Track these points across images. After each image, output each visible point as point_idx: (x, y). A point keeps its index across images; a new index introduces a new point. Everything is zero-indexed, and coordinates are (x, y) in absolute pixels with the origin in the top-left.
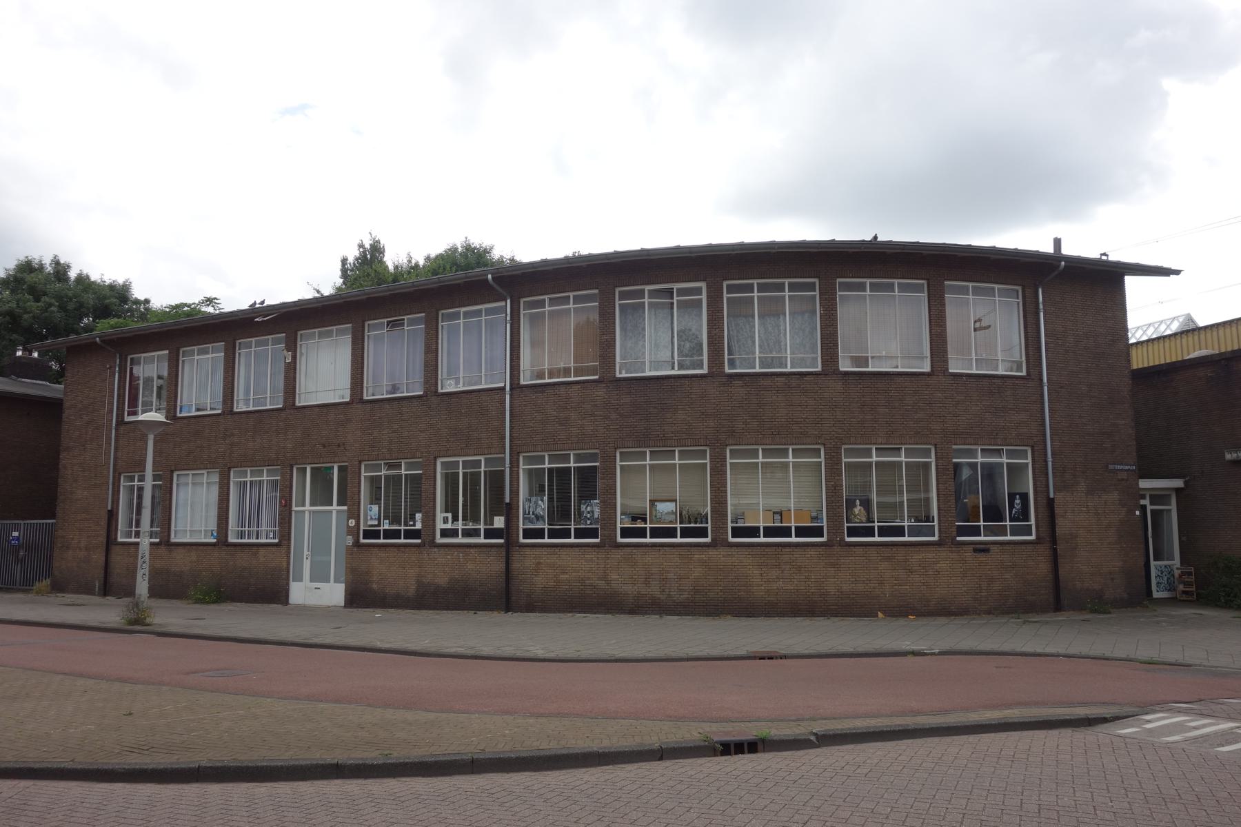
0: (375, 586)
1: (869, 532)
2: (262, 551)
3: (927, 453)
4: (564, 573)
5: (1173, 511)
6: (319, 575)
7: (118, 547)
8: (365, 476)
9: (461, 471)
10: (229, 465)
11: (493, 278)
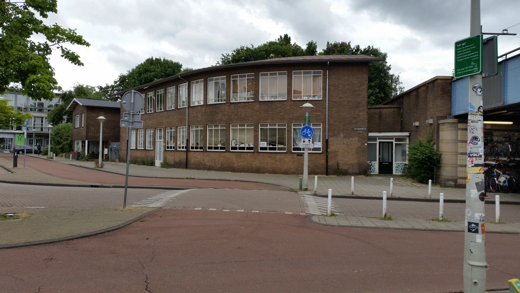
0: (167, 162)
3: (284, 125)
5: (377, 144)
7: (190, 152)
8: (208, 129)
10: (166, 127)
11: (180, 77)
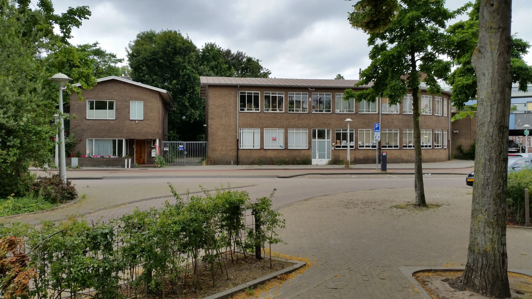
1: (363, 146)
2: (302, 151)
4: (392, 155)
6: (322, 157)
9: (253, 95)
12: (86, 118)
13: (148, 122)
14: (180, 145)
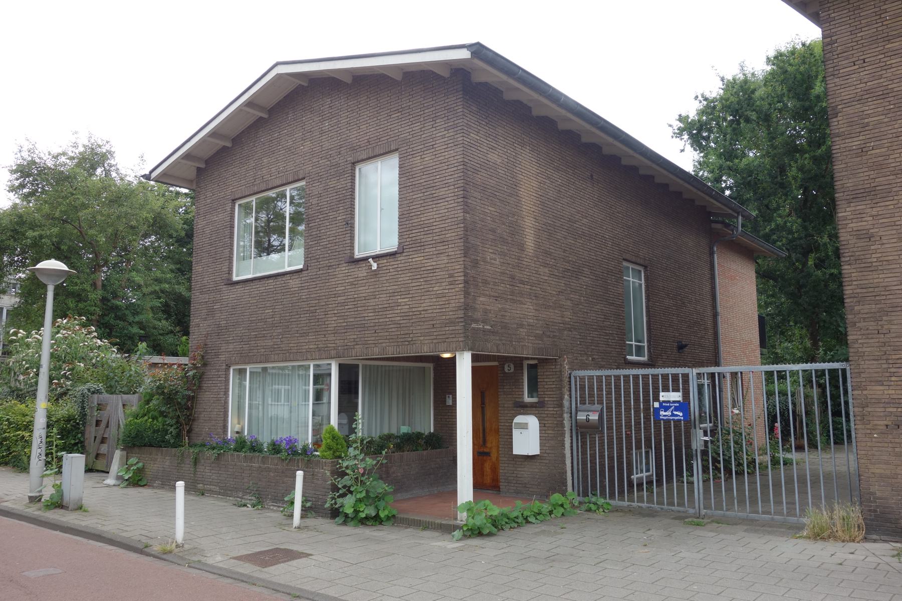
12: (230, 279)
13: (417, 258)
14: (666, 389)
